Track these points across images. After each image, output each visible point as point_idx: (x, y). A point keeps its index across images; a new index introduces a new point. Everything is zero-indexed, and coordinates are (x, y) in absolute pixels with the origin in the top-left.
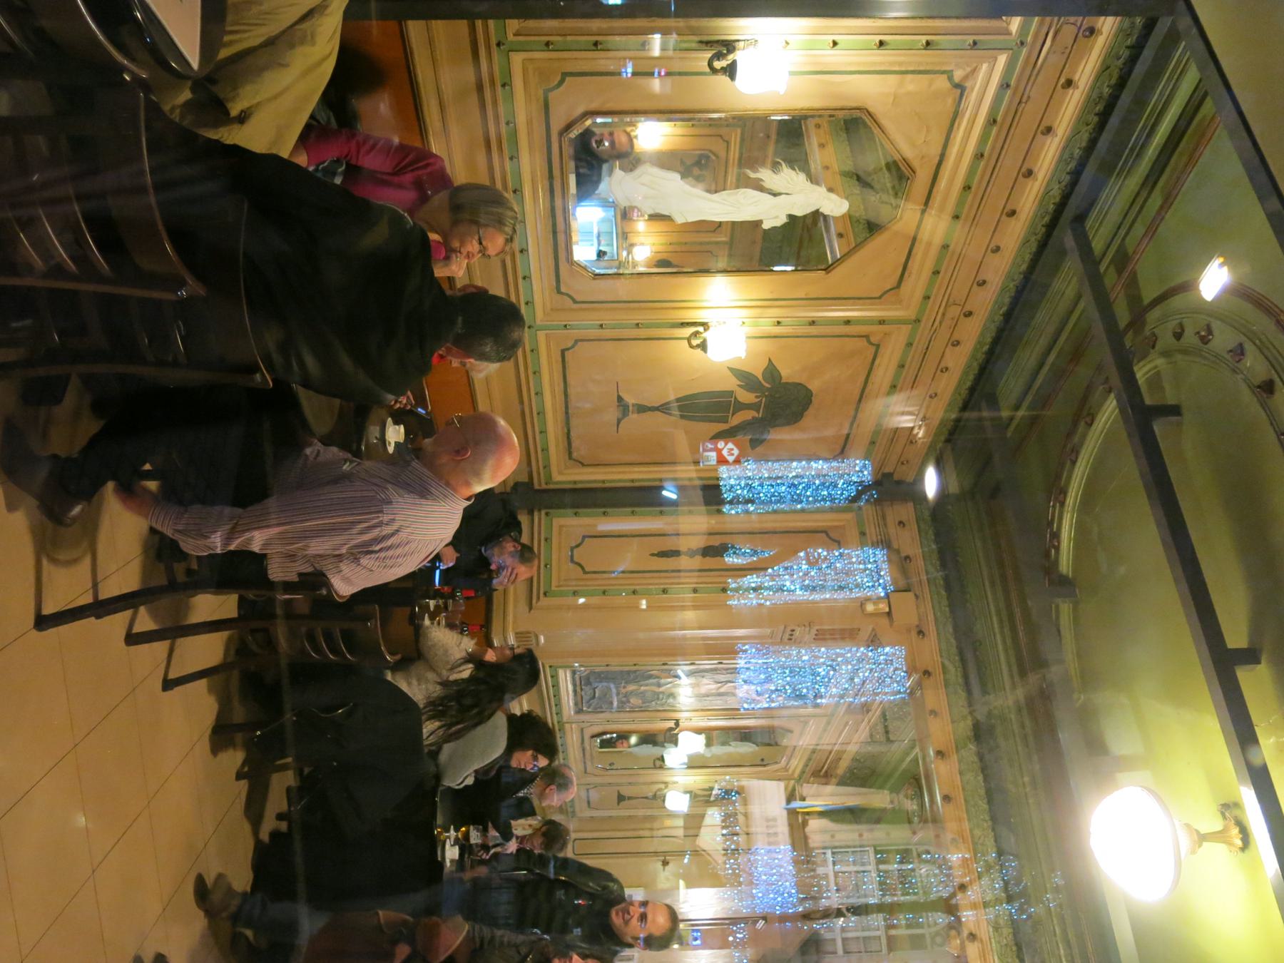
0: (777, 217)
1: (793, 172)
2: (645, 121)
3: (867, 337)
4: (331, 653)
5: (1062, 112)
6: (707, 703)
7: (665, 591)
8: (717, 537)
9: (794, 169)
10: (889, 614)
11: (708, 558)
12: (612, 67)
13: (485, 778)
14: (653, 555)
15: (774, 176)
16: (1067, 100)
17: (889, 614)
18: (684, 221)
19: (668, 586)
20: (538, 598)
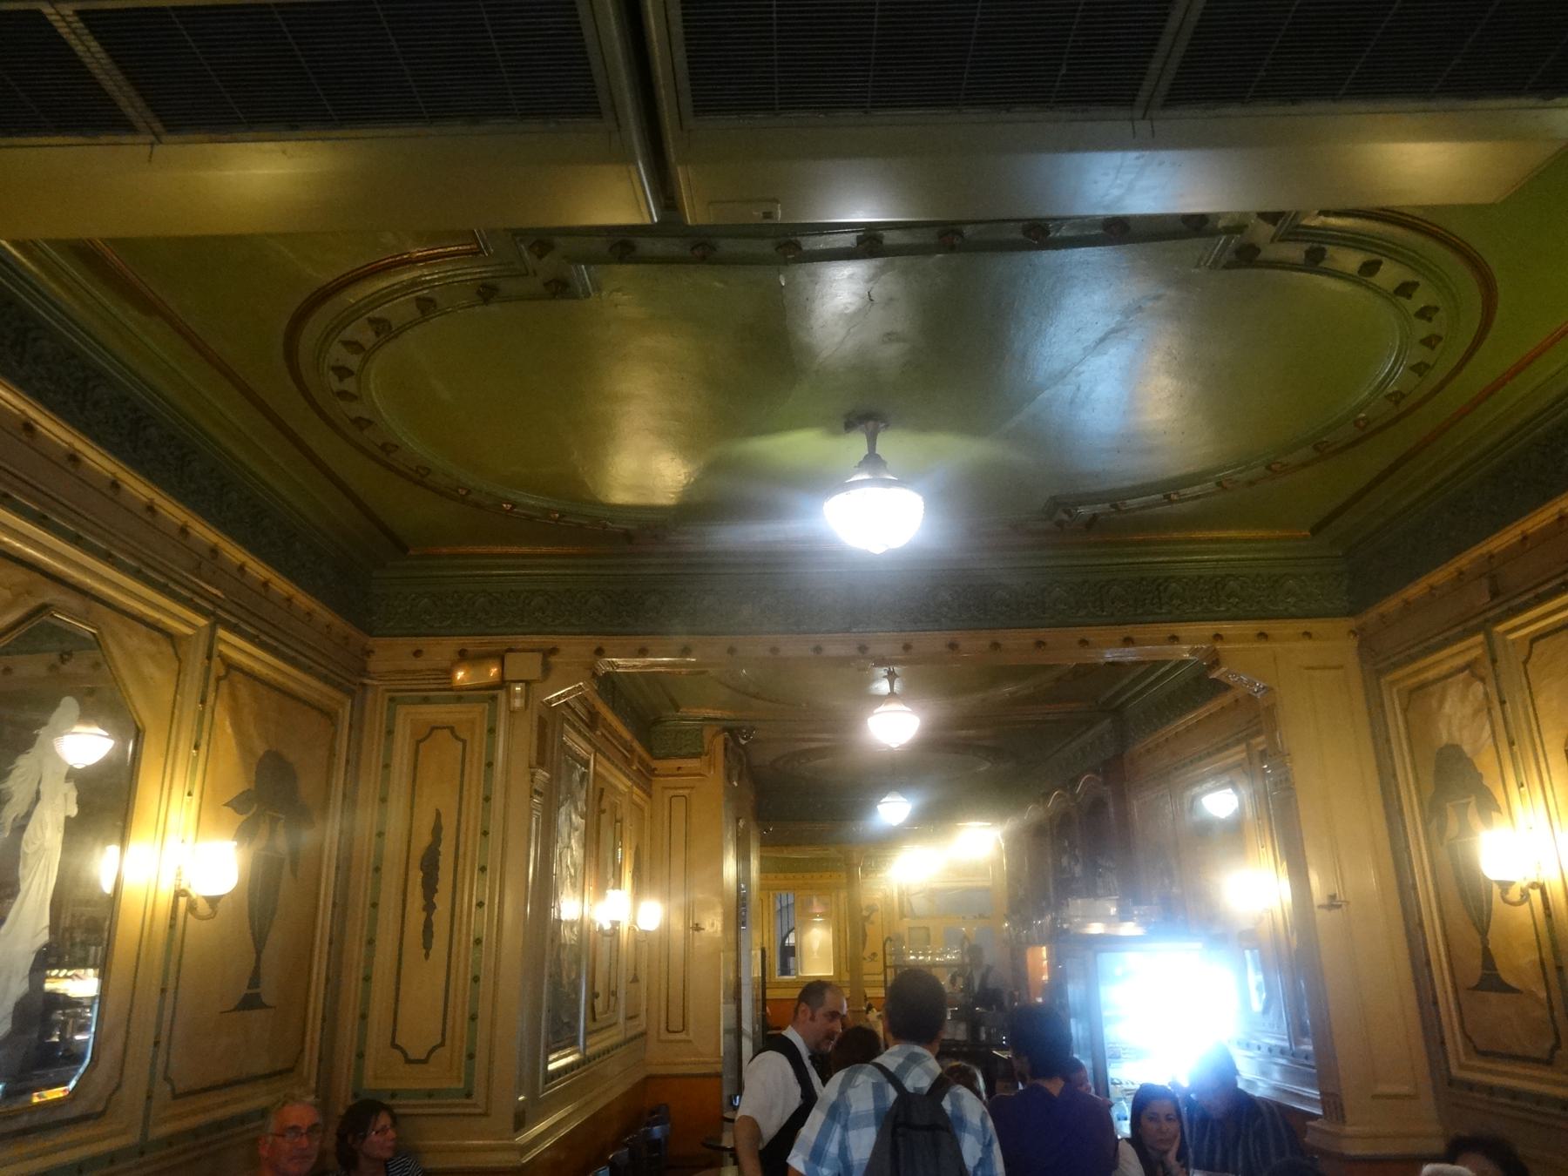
0: (66, 795)
1: (14, 772)
2: (81, 998)
3: (218, 679)
4: (957, 1067)
5: (56, 439)
6: (579, 884)
7: (478, 942)
8: (411, 874)
9: (10, 771)
10: (527, 683)
11: (438, 887)
12: (1040, 1000)
13: (918, 1049)
14: (427, 956)
15: (14, 800)
16: (92, 464)
17: (527, 683)
18: (47, 931)
19: (472, 938)
20: (475, 1105)
